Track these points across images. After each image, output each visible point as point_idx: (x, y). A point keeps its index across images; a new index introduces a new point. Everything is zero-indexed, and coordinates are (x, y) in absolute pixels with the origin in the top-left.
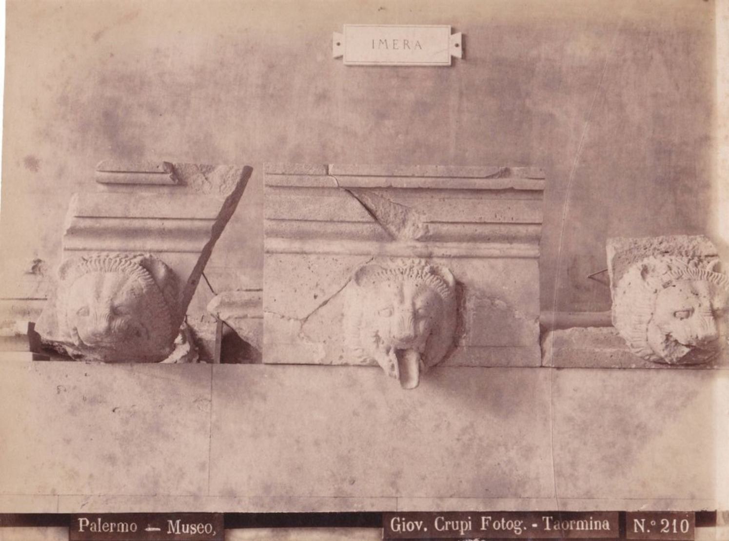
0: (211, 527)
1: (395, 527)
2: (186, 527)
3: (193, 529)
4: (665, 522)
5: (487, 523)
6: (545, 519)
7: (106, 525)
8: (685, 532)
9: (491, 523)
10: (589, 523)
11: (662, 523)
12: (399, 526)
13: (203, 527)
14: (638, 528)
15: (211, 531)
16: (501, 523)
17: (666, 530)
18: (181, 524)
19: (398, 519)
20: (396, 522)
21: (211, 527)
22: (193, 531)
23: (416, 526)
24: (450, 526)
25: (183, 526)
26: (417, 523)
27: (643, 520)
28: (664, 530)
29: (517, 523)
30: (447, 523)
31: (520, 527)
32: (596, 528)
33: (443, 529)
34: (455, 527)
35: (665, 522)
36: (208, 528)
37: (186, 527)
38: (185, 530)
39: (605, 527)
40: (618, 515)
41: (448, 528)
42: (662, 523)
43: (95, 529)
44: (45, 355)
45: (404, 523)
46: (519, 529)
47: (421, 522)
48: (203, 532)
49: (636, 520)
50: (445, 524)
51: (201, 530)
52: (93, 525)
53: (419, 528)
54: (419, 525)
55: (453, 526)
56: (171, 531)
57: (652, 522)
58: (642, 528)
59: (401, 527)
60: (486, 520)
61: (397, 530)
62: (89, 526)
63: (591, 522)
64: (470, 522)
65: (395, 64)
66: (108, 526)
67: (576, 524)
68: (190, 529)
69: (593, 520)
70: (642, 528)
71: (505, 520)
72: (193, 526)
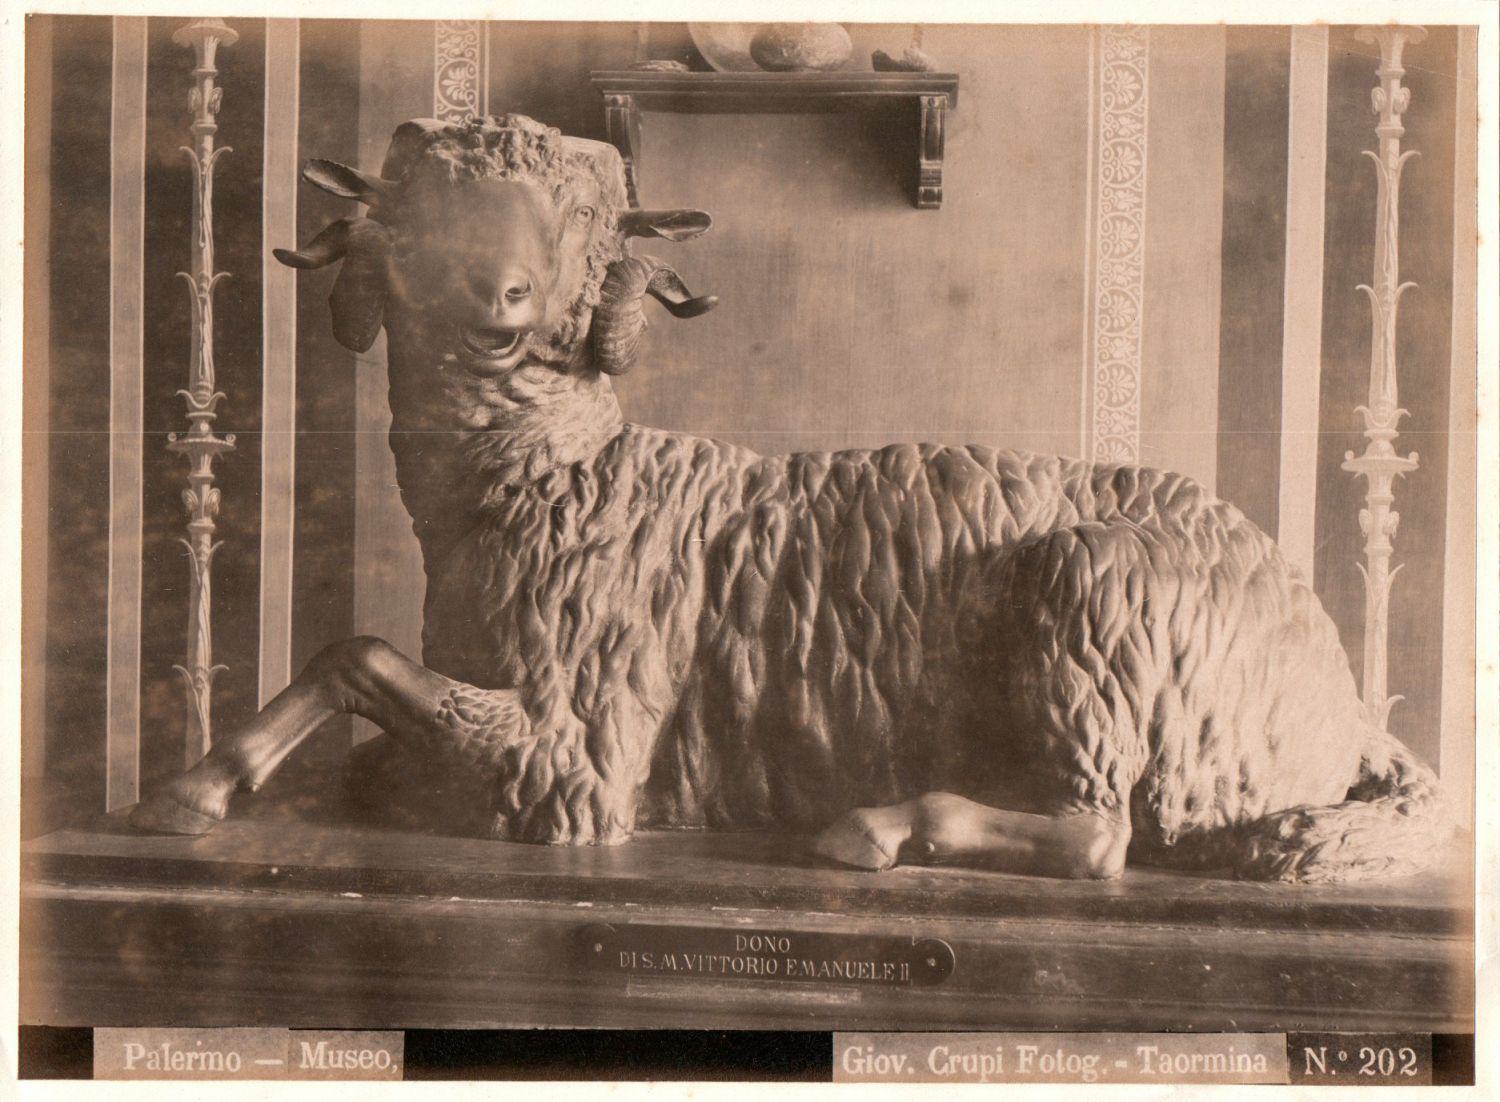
0: (238, 1058)
1: (852, 1065)
2: (336, 1055)
3: (349, 1058)
4: (1367, 1054)
5: (1030, 1059)
6: (1143, 1052)
7: (178, 1057)
8: (233, 1053)
9: (1037, 1058)
10: (996, 1059)
11: (1362, 1056)
12: (859, 1062)
13: (371, 1057)
14: (1314, 1065)
15: (388, 1064)
16: (1056, 1059)
17: (1412, 1068)
18: (327, 1048)
19: (859, 1050)
20: (854, 1054)
21: (238, 1058)
22: (351, 1063)
23: (892, 1069)
24: (959, 1066)
25: (331, 1053)
26: (894, 1057)
27: (1323, 1049)
28: (1364, 1069)
29: (1089, 1061)
30: (952, 1059)
31: (1095, 1068)
32: (974, 1057)
33: (945, 1069)
34: (970, 1067)
35: (1367, 1054)
36: (383, 1061)
37: (336, 1055)
38: (336, 1062)
39: (1260, 1067)
40: (98, 1063)
41: (193, 1066)
42: (1362, 1056)
43: (158, 1064)
44: (1258, 1019)
45: (870, 1057)
46: (1093, 1072)
47: (904, 1057)
48: (371, 1064)
49: (1309, 1051)
50: (948, 1061)
51: (367, 1062)
52: (1166, 1059)
53: (898, 1069)
54: (1319, 1056)
55: (965, 1066)
56: (308, 1062)
57: (1345, 1055)
58: (1322, 1067)
59: (864, 1065)
60: (1027, 1053)
61: (857, 1071)
62: (146, 1059)
63: (1232, 1057)
64: (1000, 1058)
65: (898, 1036)
66: (182, 1059)
67: (199, 1060)
68: (344, 1060)
69: (1237, 1053)
70: (1322, 1067)
71: (1064, 1053)
72: (351, 1055)
